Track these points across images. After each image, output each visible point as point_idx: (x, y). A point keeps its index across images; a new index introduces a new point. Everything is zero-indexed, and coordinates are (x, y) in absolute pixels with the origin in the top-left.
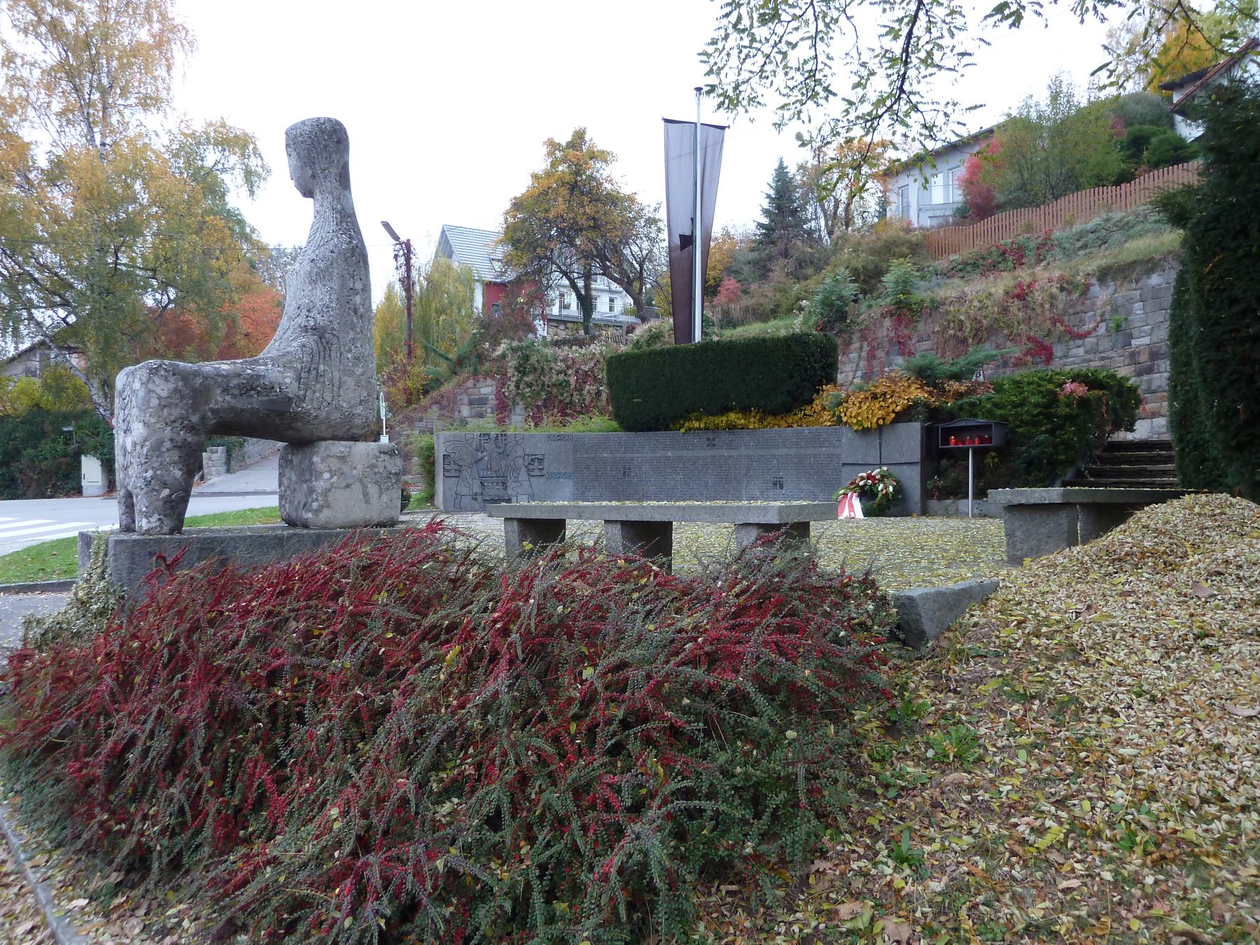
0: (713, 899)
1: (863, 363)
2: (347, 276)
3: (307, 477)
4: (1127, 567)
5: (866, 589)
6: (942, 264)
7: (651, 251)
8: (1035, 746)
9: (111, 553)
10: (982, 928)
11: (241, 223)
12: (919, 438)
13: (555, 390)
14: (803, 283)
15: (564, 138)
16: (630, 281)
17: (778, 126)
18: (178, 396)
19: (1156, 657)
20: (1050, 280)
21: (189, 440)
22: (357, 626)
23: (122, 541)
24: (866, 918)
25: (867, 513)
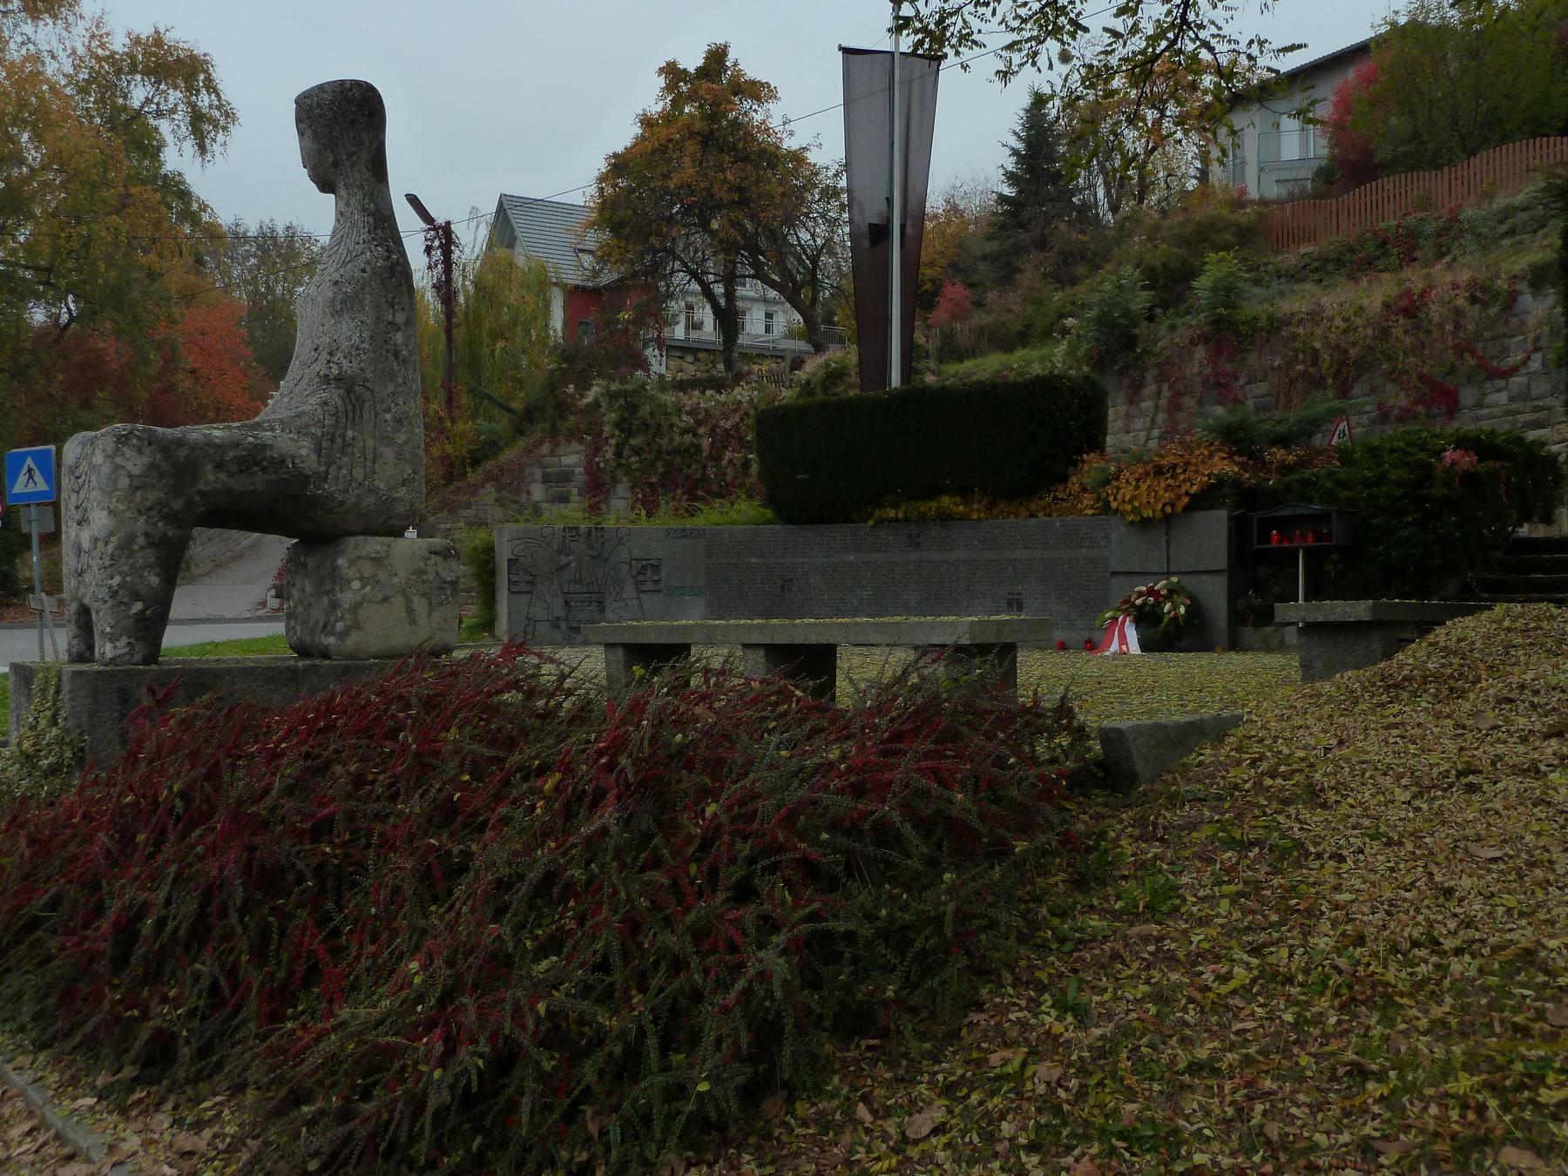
0: (851, 1054)
1: (1161, 417)
2: (385, 306)
3: (328, 586)
4: (1405, 695)
5: (1061, 718)
6: (1289, 259)
7: (828, 240)
8: (1241, 894)
9: (66, 688)
10: (1140, 1067)
11: (184, 195)
12: (1224, 533)
13: (678, 459)
14: (1069, 291)
15: (692, 61)
16: (797, 286)
17: (1005, 75)
18: (155, 473)
19: (1406, 796)
20: (1455, 286)
21: (170, 534)
22: (424, 766)
23: (82, 673)
24: (1017, 1063)
25: (1145, 646)
